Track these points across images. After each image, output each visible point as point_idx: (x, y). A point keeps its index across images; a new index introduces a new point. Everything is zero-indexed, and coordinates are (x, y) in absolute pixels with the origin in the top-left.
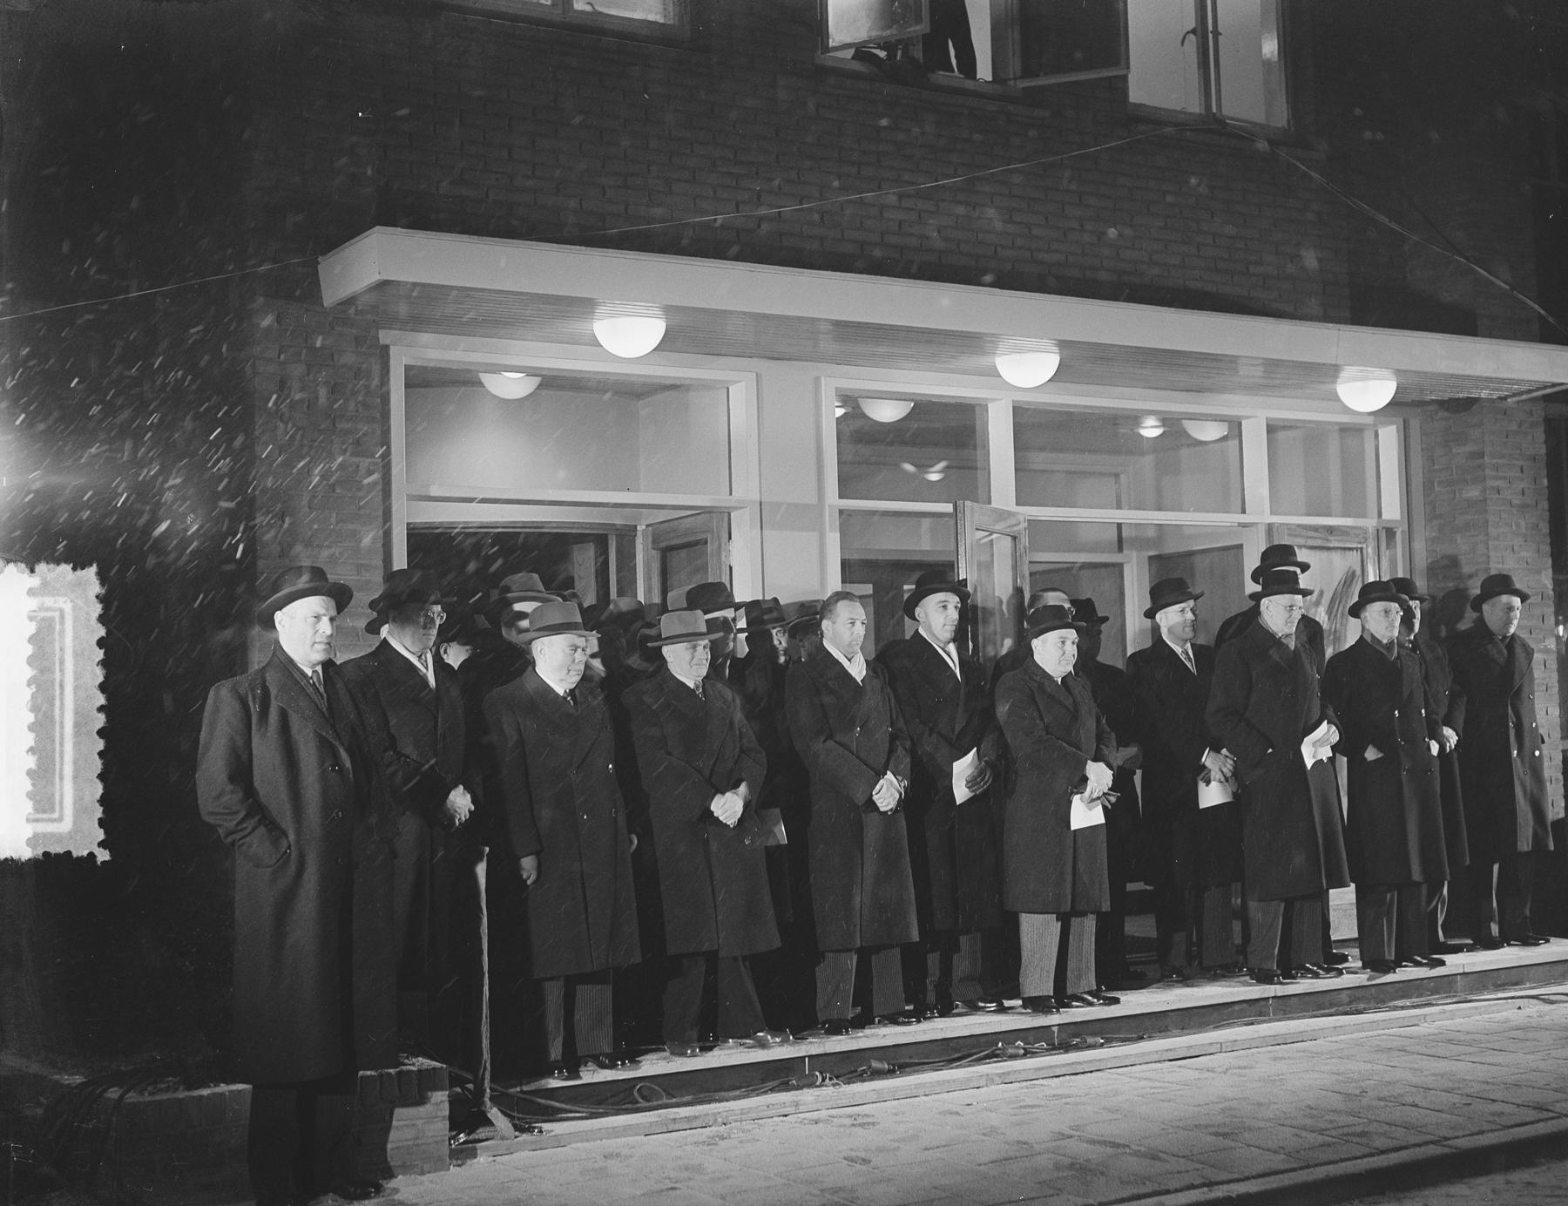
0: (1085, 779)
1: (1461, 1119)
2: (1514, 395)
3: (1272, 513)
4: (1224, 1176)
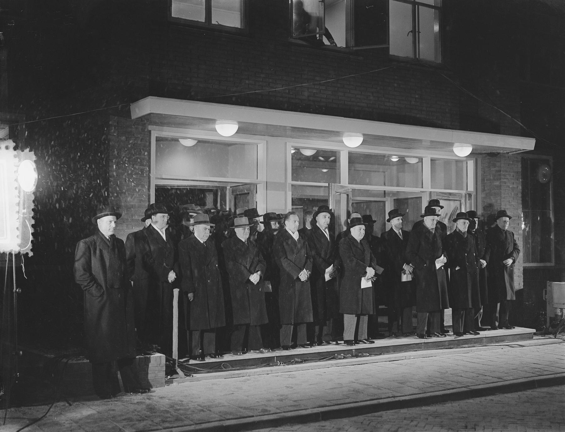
0: (366, 273)
1: (474, 381)
2: (511, 152)
3: (431, 188)
4: (399, 395)
